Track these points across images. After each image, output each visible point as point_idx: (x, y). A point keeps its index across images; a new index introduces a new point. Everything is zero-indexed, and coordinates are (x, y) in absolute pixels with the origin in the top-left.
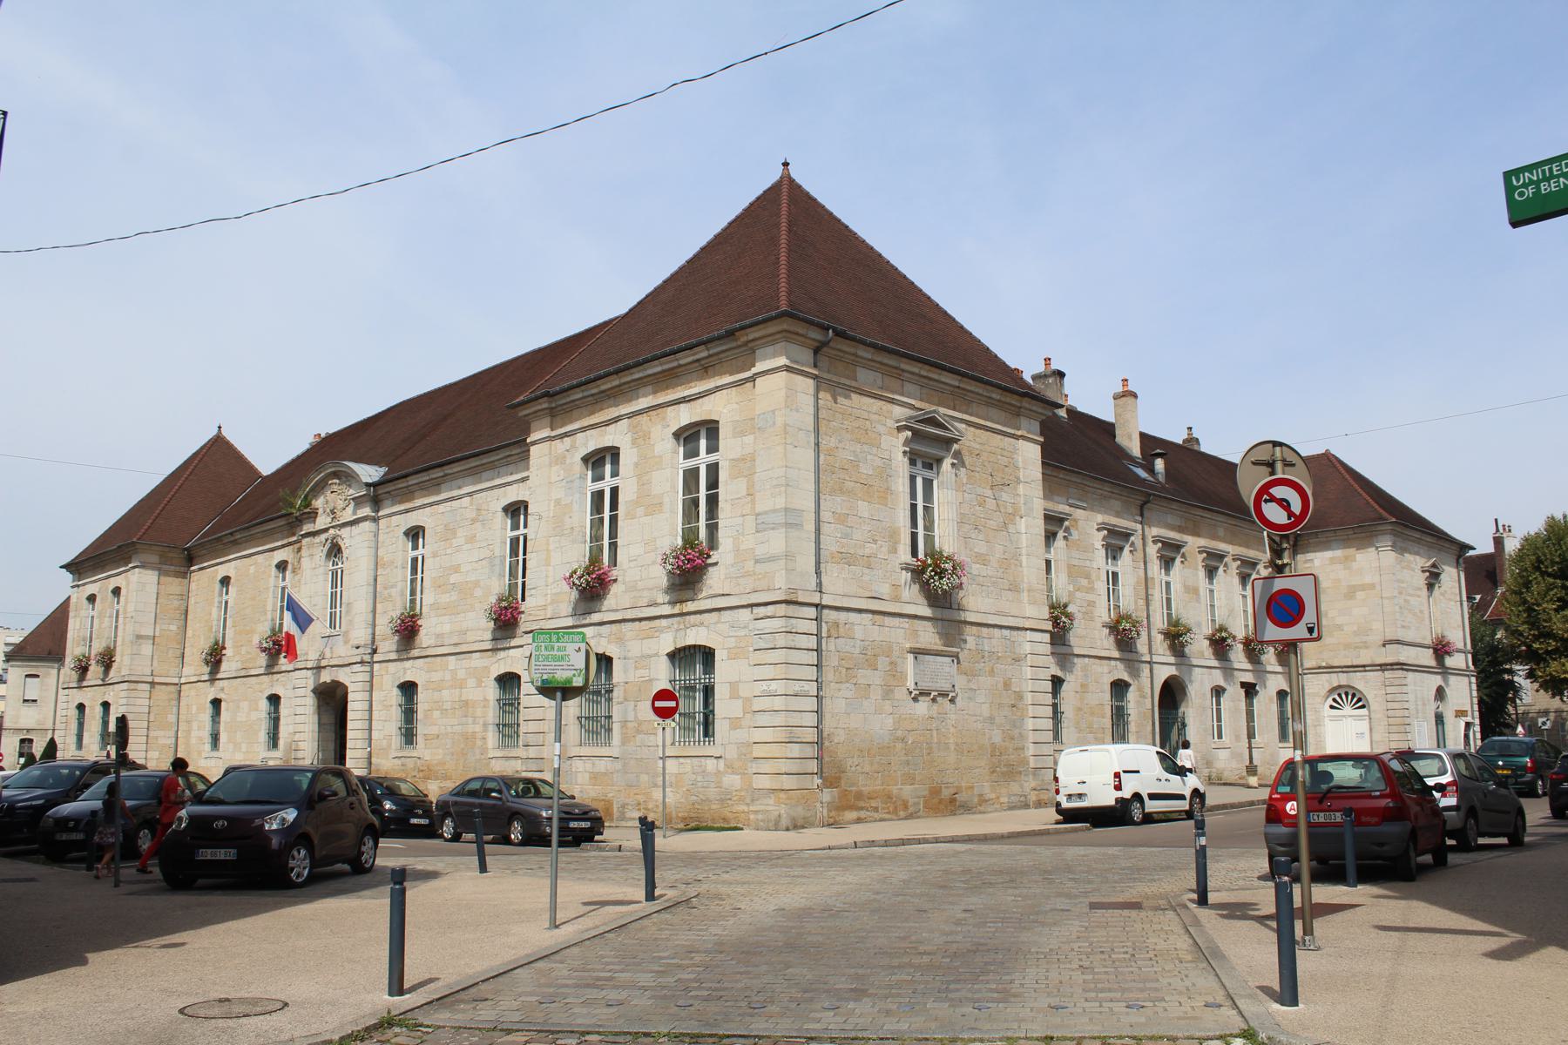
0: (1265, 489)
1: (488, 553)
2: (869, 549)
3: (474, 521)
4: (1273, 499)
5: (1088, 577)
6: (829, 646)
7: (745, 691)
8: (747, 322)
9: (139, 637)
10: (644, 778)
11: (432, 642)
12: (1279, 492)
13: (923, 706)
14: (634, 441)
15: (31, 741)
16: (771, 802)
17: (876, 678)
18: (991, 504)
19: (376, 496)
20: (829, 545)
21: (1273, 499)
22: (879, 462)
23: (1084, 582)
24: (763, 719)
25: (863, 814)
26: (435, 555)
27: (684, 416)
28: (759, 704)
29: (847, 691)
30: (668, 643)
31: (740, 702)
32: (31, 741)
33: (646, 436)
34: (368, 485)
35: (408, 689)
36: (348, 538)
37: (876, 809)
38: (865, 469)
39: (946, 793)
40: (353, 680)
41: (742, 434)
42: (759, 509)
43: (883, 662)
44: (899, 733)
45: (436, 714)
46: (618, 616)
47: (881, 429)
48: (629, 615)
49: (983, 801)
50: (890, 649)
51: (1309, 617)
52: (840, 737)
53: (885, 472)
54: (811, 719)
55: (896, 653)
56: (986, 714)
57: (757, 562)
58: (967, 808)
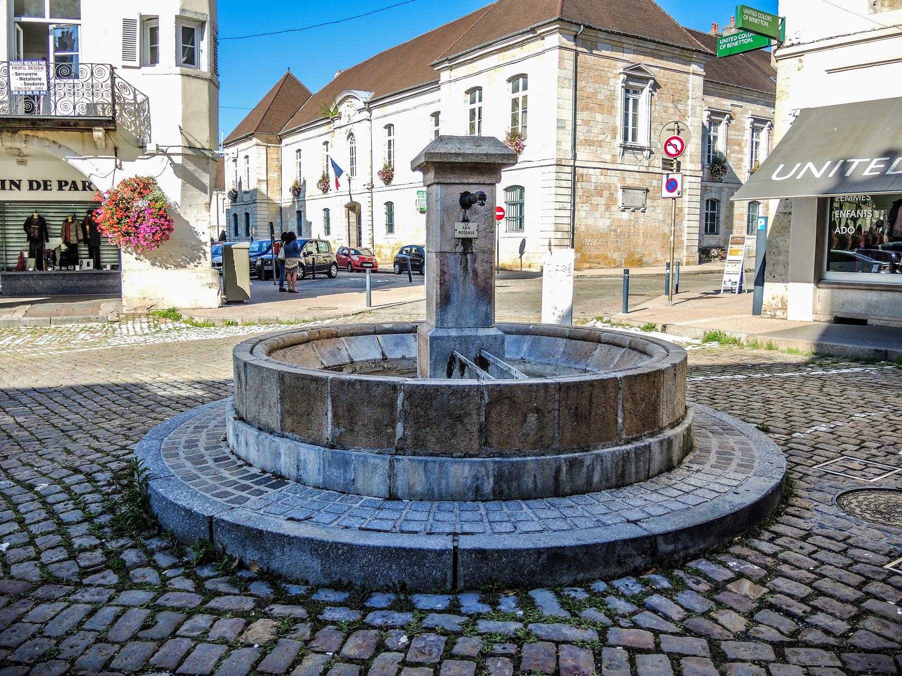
0: (669, 141)
2: (601, 137)
4: (671, 144)
5: (740, 145)
6: (579, 185)
8: (540, 24)
9: (260, 181)
12: (674, 142)
13: (626, 215)
17: (602, 201)
18: (671, 111)
19: (369, 106)
20: (580, 136)
21: (671, 144)
22: (608, 93)
23: (737, 148)
25: (592, 265)
29: (586, 207)
35: (389, 205)
36: (357, 129)
37: (599, 263)
38: (600, 97)
39: (637, 256)
40: (363, 200)
43: (606, 193)
44: (613, 227)
47: (610, 75)
49: (657, 261)
50: (610, 187)
51: (679, 189)
52: (583, 228)
53: (611, 98)
54: (567, 221)
55: (613, 189)
58: (648, 265)
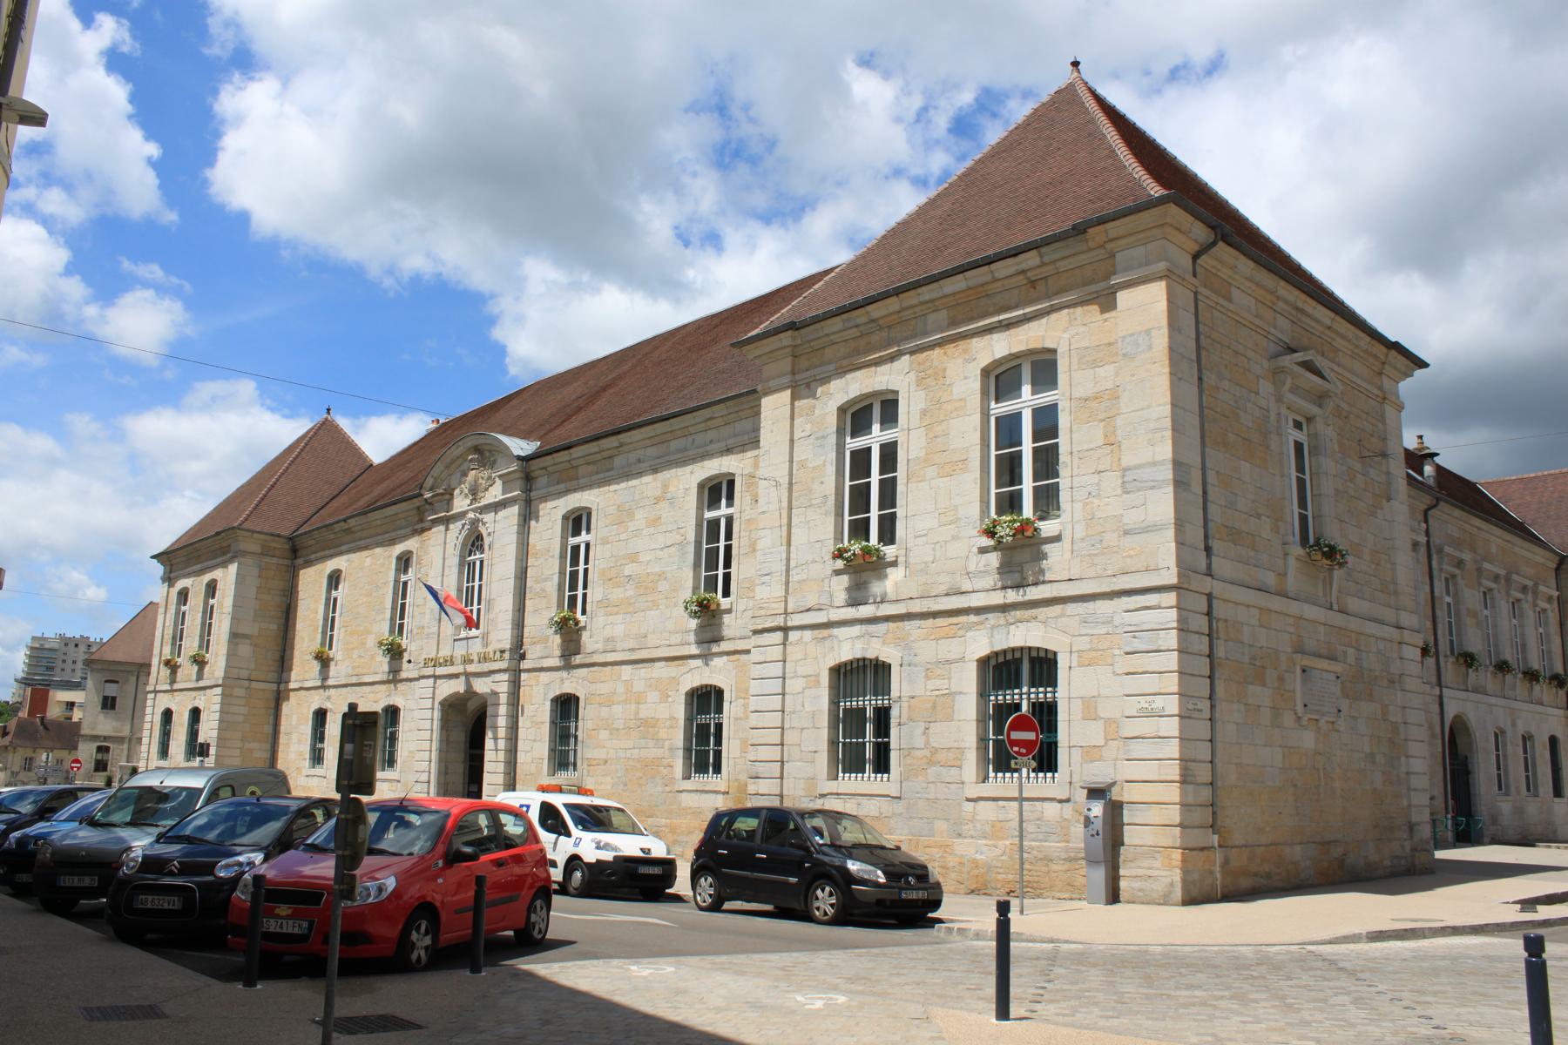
1: (679, 538)
3: (658, 500)
7: (1106, 710)
10: (940, 825)
11: (600, 646)
14: (920, 382)
15: (1043, 666)
16: (1157, 864)
24: (1139, 749)
26: (605, 541)
27: (1000, 346)
28: (1131, 728)
30: (983, 641)
31: (1100, 724)
32: (1043, 666)
33: (940, 374)
34: (519, 458)
41: (1095, 364)
42: (1125, 463)
45: (604, 734)
46: (900, 609)
48: (916, 607)
56: (1367, 750)
57: (1126, 533)
